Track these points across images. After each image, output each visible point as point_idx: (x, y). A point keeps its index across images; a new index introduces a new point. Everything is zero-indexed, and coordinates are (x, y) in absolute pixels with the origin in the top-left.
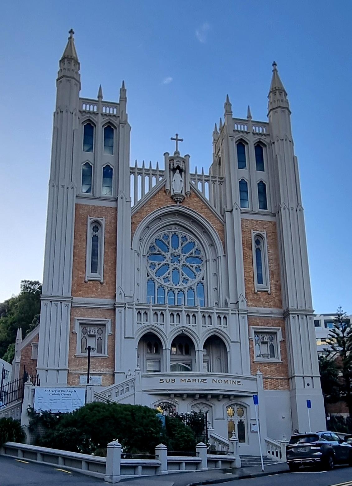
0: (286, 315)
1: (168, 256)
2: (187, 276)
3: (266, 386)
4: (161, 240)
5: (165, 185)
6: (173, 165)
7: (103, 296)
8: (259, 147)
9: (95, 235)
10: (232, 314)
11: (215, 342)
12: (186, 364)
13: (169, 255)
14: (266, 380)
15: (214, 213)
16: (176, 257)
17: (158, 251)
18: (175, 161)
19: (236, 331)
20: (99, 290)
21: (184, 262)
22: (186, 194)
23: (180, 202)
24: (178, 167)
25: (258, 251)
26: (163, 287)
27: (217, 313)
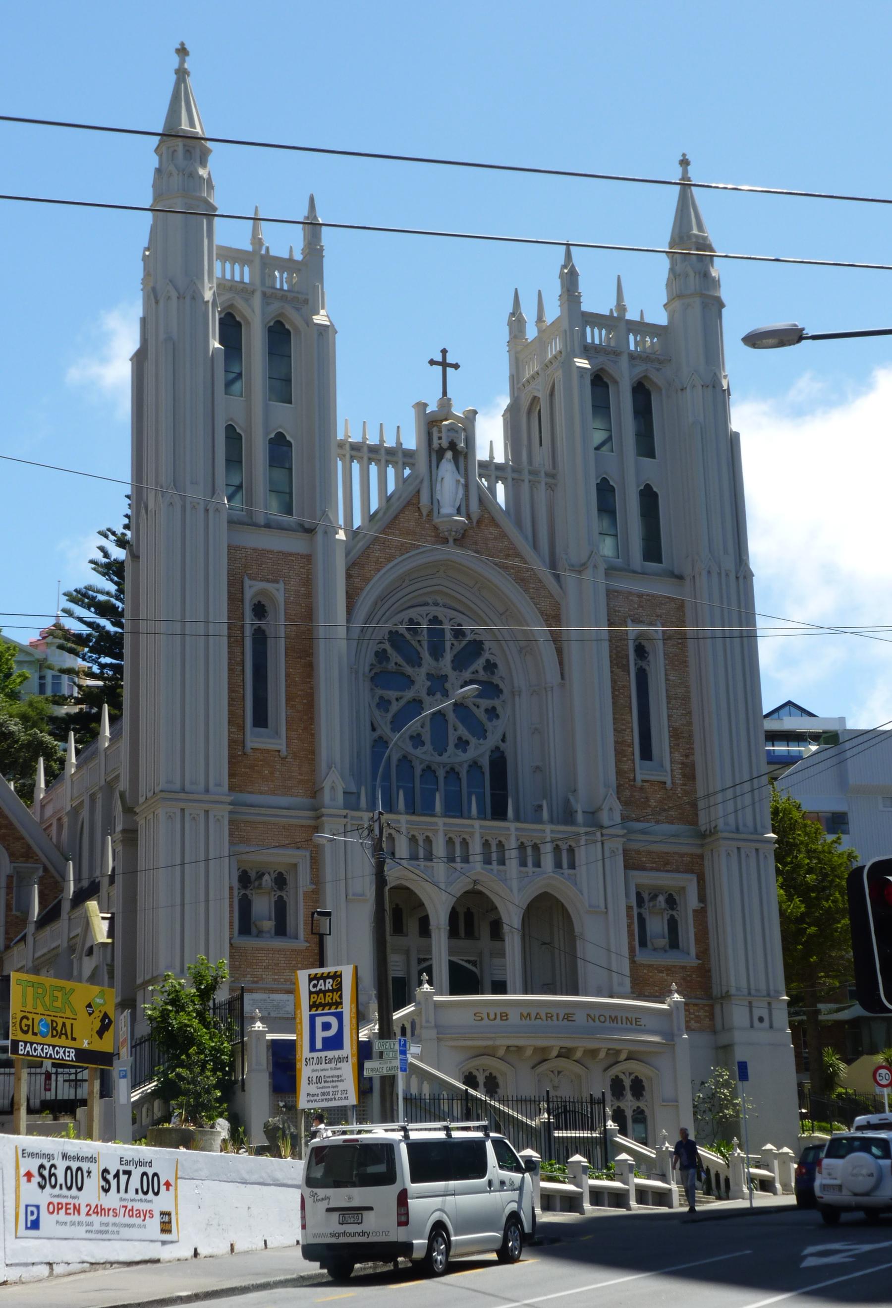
0: (704, 836)
2: (467, 733)
5: (418, 492)
6: (440, 438)
8: (642, 393)
11: (546, 911)
12: (468, 961)
13: (423, 676)
20: (277, 774)
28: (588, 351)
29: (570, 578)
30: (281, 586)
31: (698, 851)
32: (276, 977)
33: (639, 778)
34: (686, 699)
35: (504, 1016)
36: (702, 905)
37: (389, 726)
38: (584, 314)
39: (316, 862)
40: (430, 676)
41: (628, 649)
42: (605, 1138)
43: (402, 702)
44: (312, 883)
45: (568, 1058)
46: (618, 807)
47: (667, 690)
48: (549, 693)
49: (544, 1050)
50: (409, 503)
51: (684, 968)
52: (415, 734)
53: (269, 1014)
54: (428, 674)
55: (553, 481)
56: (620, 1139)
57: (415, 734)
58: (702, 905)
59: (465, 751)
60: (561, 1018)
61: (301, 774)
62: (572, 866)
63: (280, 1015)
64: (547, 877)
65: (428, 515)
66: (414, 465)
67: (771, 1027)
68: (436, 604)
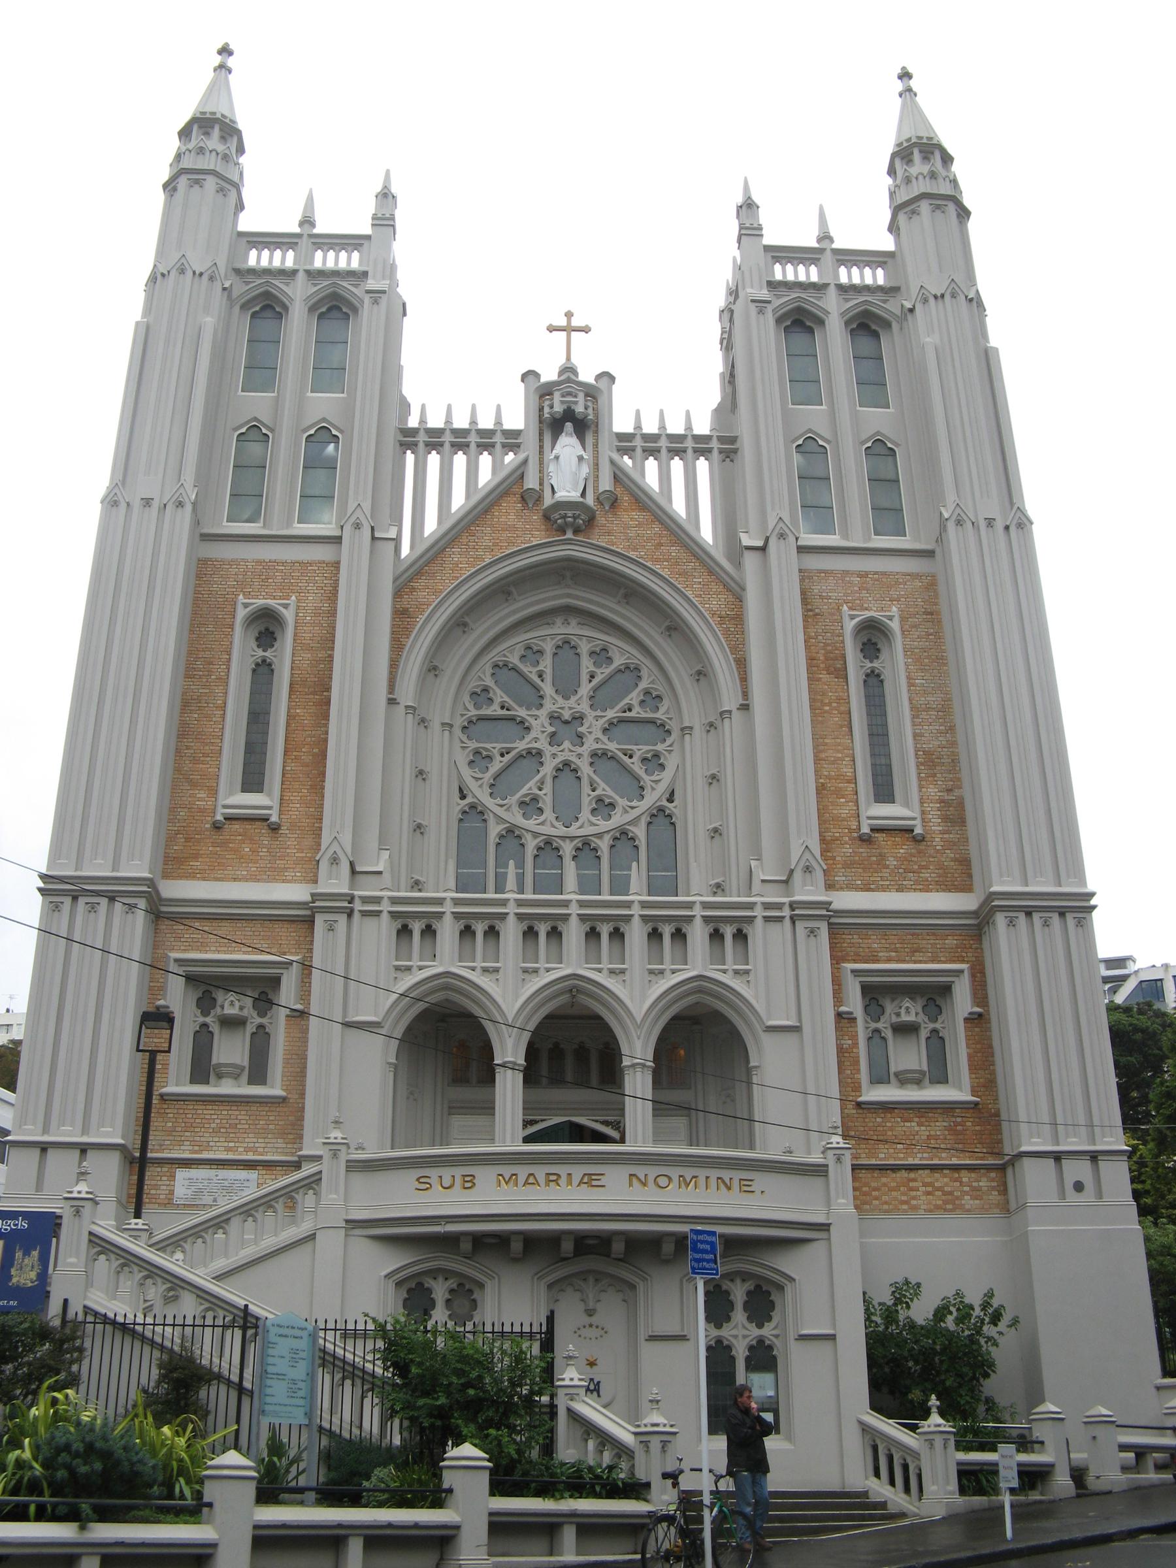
1: (540, 724)
2: (610, 792)
3: (914, 1198)
4: (514, 669)
5: (522, 477)
6: (552, 407)
7: (275, 875)
9: (264, 661)
10: (767, 919)
14: (912, 1175)
15: (704, 556)
16: (567, 726)
17: (502, 708)
18: (557, 397)
19: (784, 990)
21: (597, 740)
22: (598, 500)
23: (577, 531)
24: (568, 414)
25: (873, 680)
26: (519, 837)
27: (707, 920)
32: (232, 1144)
39: (307, 967)
47: (910, 700)
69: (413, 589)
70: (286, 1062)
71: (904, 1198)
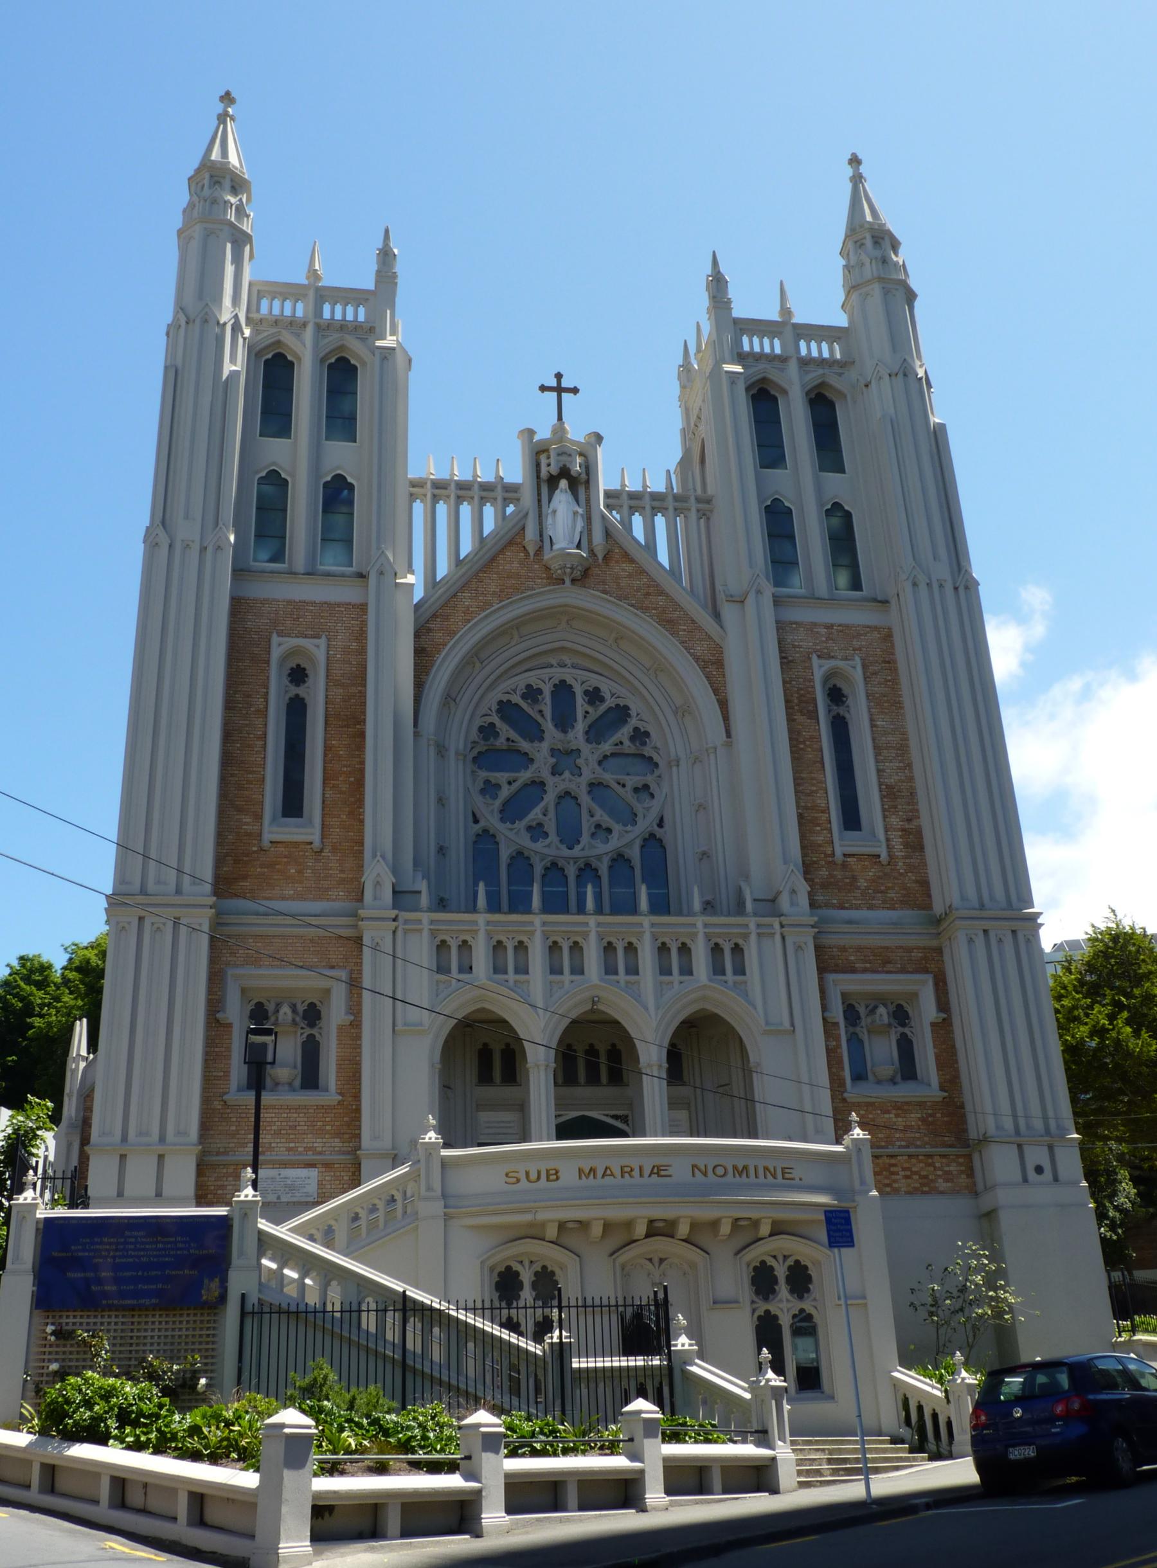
5: (523, 529)
12: (616, 1117)
13: (586, 771)
14: (893, 1161)
28: (741, 357)
29: (729, 612)
30: (322, 642)
31: (934, 943)
32: (292, 1145)
33: (839, 851)
34: (903, 749)
35: (553, 1175)
36: (945, 1016)
37: (497, 816)
38: (736, 321)
39: (354, 985)
40: (553, 752)
41: (814, 693)
42: (670, 1368)
43: (516, 786)
44: (347, 1013)
45: (672, 1237)
46: (803, 888)
47: (874, 739)
48: (712, 756)
49: (629, 1225)
50: (511, 543)
51: (921, 1105)
52: (534, 824)
53: (279, 1198)
54: (552, 750)
55: (707, 506)
56: (699, 1369)
57: (534, 824)
58: (945, 1016)
59: (607, 841)
60: (647, 1172)
61: (342, 871)
62: (740, 970)
63: (295, 1199)
64: (700, 987)
65: (536, 554)
66: (518, 500)
67: (1056, 1179)
68: (563, 665)
69: (429, 630)
70: (339, 1067)
71: (887, 1181)
